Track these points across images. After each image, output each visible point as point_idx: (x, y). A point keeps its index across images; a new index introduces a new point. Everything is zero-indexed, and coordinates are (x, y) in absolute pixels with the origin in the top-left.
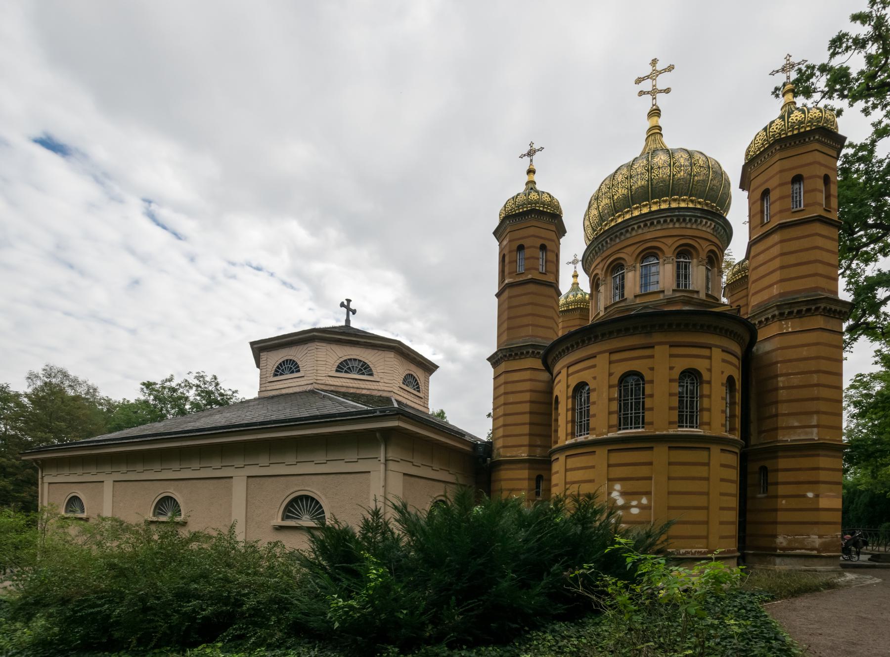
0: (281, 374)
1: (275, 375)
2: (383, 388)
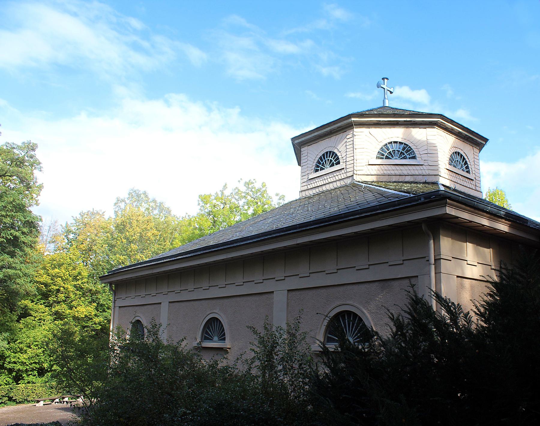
0: (322, 169)
1: (317, 171)
2: (428, 172)
